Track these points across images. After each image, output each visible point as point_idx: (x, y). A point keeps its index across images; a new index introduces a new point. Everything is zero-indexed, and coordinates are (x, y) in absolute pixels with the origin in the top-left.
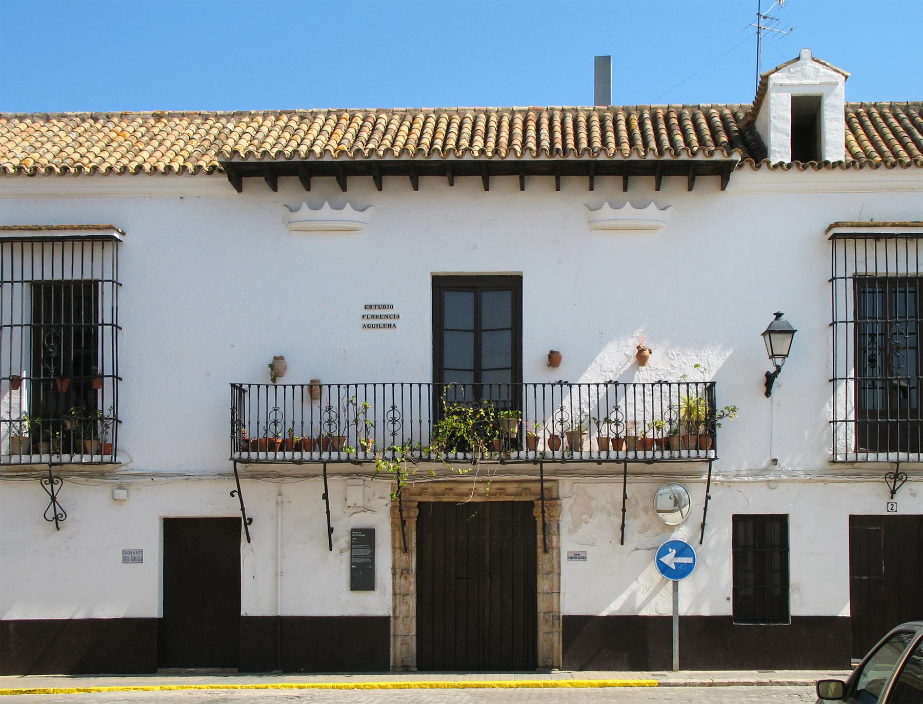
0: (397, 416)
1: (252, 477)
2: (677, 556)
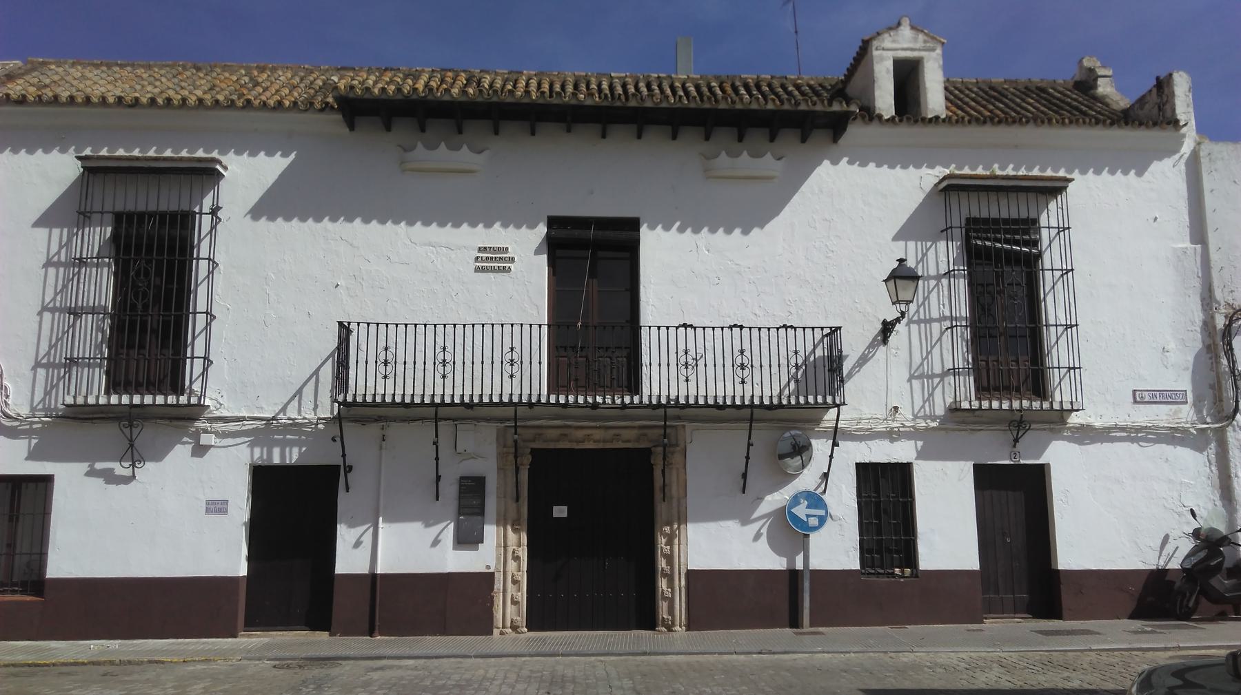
0: (516, 357)
1: (356, 421)
2: (808, 507)
